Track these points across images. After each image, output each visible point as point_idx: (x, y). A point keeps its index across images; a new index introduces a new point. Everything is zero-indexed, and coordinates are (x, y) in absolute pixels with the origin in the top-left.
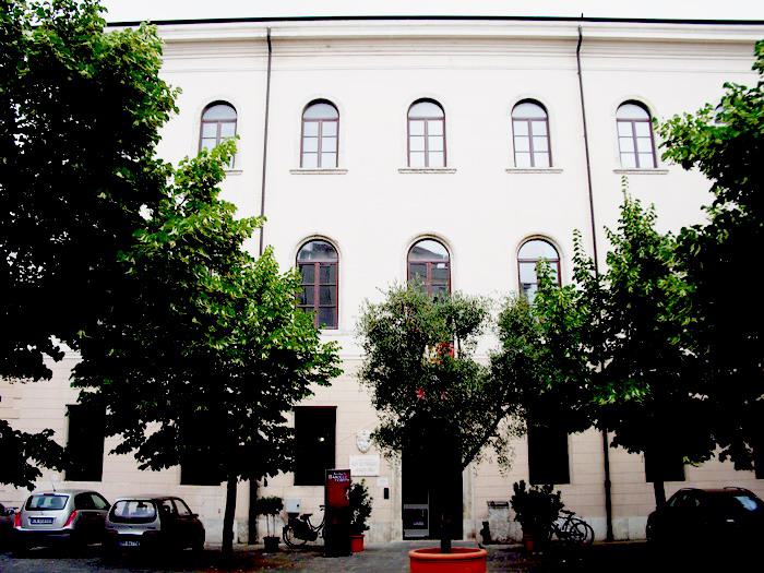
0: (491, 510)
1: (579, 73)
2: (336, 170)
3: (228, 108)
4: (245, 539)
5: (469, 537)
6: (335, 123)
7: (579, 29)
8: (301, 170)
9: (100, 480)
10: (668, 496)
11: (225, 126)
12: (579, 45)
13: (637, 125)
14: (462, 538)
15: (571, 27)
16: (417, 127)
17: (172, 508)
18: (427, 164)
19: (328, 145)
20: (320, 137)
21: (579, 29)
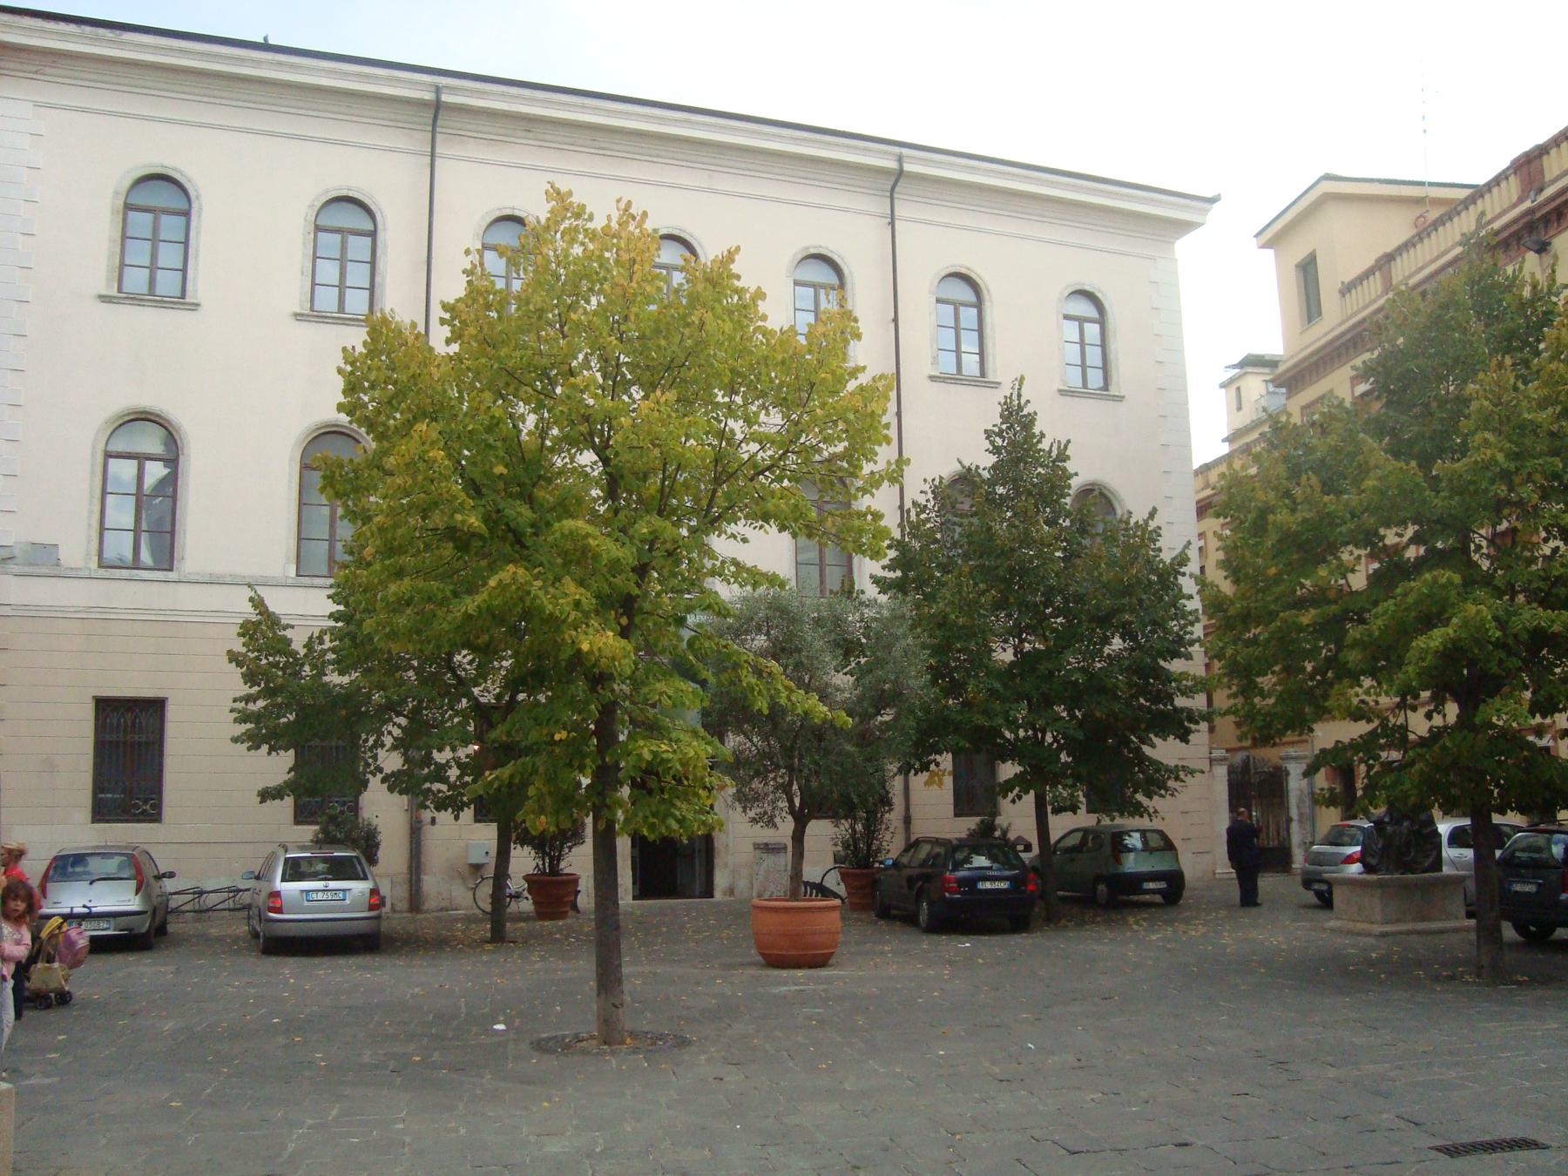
0: (764, 856)
1: (892, 224)
2: (181, 300)
3: (175, 188)
4: (403, 905)
5: (725, 893)
6: (369, 239)
7: (900, 159)
8: (120, 296)
9: (94, 821)
10: (1054, 836)
11: (166, 220)
12: (897, 181)
13: (1087, 326)
14: (1440, 870)
15: (886, 153)
16: (141, 221)
17: (937, 850)
18: (341, 308)
19: (169, 256)
20: (155, 241)
21: (900, 159)
